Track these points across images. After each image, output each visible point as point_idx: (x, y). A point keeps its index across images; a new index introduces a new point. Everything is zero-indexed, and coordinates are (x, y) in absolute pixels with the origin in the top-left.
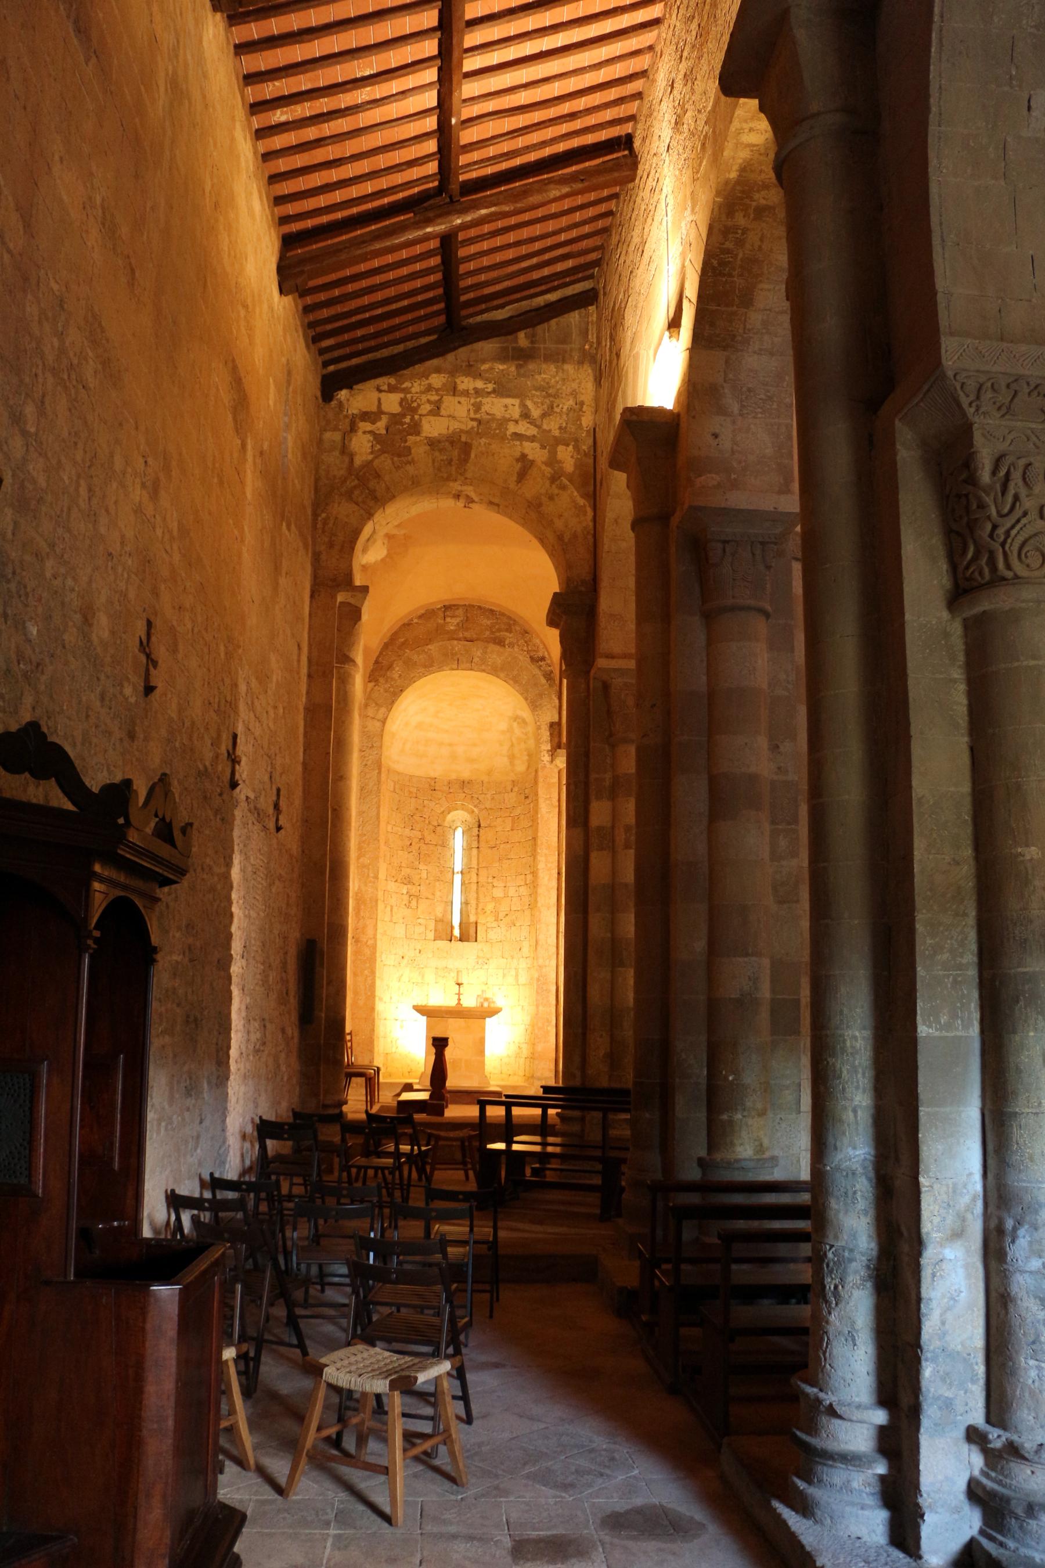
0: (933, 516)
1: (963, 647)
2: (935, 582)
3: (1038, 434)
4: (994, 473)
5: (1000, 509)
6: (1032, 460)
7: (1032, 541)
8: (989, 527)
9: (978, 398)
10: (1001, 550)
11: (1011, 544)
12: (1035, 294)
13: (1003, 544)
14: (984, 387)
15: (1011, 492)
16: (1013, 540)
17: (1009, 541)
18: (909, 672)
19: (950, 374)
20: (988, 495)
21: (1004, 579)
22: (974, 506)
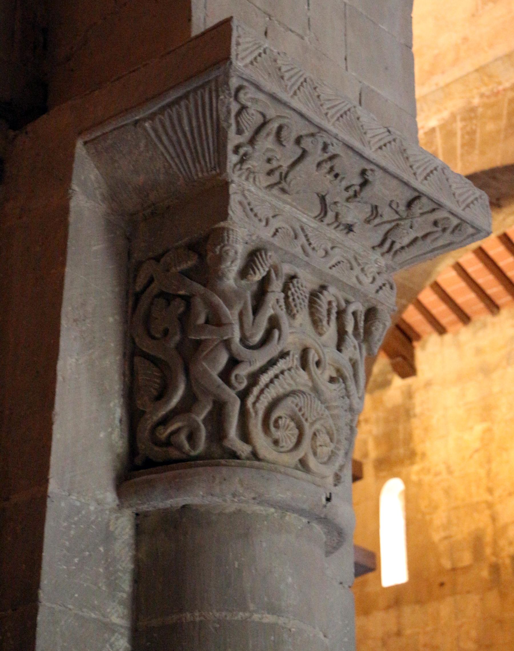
1: (131, 566)
2: (102, 435)
3: (310, 235)
4: (243, 273)
5: (248, 334)
8: (223, 359)
9: (252, 141)
10: (238, 403)
11: (258, 398)
12: (308, 32)
13: (244, 395)
15: (268, 311)
16: (262, 391)
17: (256, 391)
18: (42, 595)
19: (234, 82)
20: (230, 306)
21: (234, 455)
22: (201, 320)
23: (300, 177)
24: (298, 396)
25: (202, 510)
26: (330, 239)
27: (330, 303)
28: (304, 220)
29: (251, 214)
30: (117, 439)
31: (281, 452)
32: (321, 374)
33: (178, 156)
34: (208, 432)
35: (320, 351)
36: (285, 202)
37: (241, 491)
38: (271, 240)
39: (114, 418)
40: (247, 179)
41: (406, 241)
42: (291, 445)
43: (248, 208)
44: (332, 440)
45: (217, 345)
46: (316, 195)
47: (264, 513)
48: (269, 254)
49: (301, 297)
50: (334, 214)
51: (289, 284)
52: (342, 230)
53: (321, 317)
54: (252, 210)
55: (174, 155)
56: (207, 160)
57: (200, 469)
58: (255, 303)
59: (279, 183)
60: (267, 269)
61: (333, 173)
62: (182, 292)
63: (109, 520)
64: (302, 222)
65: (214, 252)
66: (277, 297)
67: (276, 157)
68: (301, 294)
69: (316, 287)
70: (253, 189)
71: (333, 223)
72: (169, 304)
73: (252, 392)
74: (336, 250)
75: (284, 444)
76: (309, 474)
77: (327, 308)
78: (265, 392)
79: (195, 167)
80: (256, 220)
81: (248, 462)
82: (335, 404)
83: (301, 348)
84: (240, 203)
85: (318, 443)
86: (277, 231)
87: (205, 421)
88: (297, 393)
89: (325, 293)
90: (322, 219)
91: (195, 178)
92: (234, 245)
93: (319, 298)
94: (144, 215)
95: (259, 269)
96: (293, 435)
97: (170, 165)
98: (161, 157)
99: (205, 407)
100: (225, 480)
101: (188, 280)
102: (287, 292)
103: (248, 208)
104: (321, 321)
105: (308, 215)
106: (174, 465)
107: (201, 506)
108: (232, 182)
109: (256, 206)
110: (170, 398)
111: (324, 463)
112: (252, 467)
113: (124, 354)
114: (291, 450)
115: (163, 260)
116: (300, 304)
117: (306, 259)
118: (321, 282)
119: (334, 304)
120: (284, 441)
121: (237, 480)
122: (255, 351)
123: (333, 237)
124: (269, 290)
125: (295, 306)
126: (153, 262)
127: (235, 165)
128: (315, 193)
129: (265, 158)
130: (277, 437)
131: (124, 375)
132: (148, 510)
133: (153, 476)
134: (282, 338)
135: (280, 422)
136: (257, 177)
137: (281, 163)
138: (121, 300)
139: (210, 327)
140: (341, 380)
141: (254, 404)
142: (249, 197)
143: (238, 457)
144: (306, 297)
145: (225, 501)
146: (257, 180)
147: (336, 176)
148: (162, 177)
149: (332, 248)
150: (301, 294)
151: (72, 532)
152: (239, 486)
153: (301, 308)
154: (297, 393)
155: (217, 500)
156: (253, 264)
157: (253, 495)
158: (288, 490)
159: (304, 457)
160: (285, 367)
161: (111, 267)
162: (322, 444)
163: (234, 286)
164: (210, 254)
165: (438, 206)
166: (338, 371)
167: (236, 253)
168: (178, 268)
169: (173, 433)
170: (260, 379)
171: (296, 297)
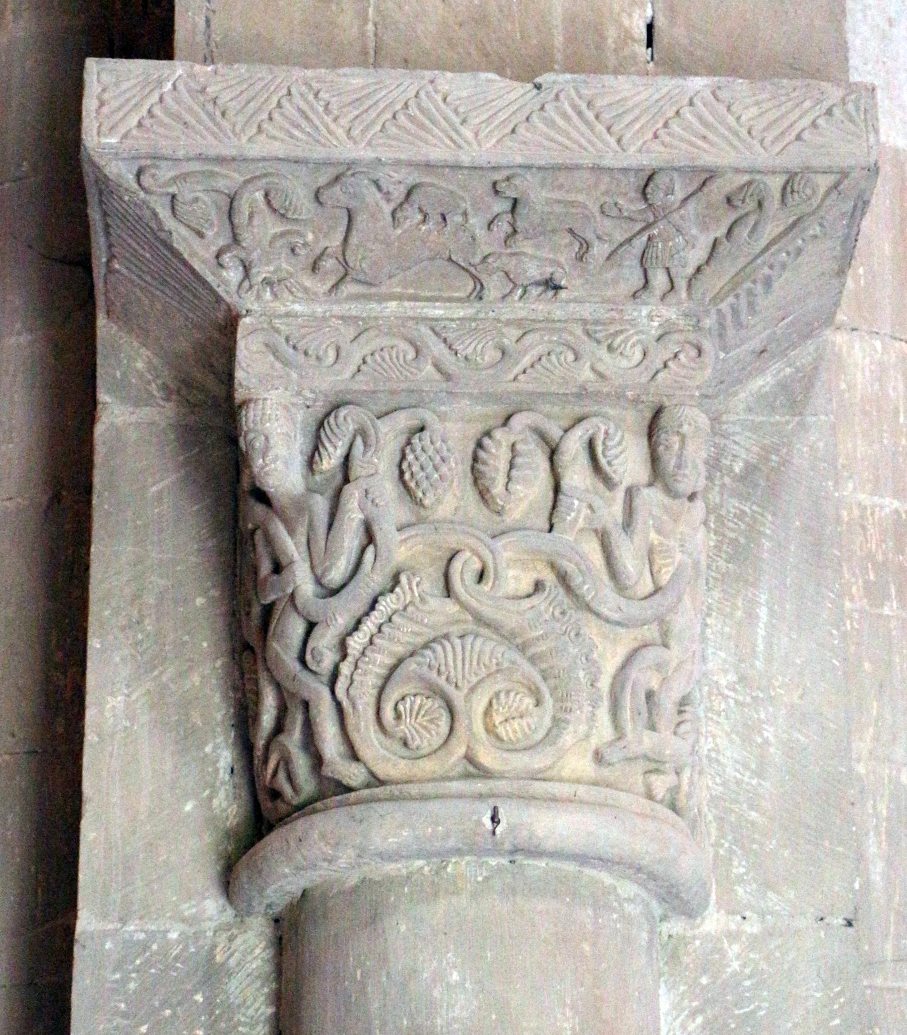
3: (451, 336)
6: (428, 416)
7: (411, 666)
14: (243, 208)
40: (275, 295)
41: (696, 256)
63: (214, 946)
75: (418, 742)
81: (365, 792)
92: (259, 427)
151: (132, 986)
161: (195, 508)
165: (709, 176)
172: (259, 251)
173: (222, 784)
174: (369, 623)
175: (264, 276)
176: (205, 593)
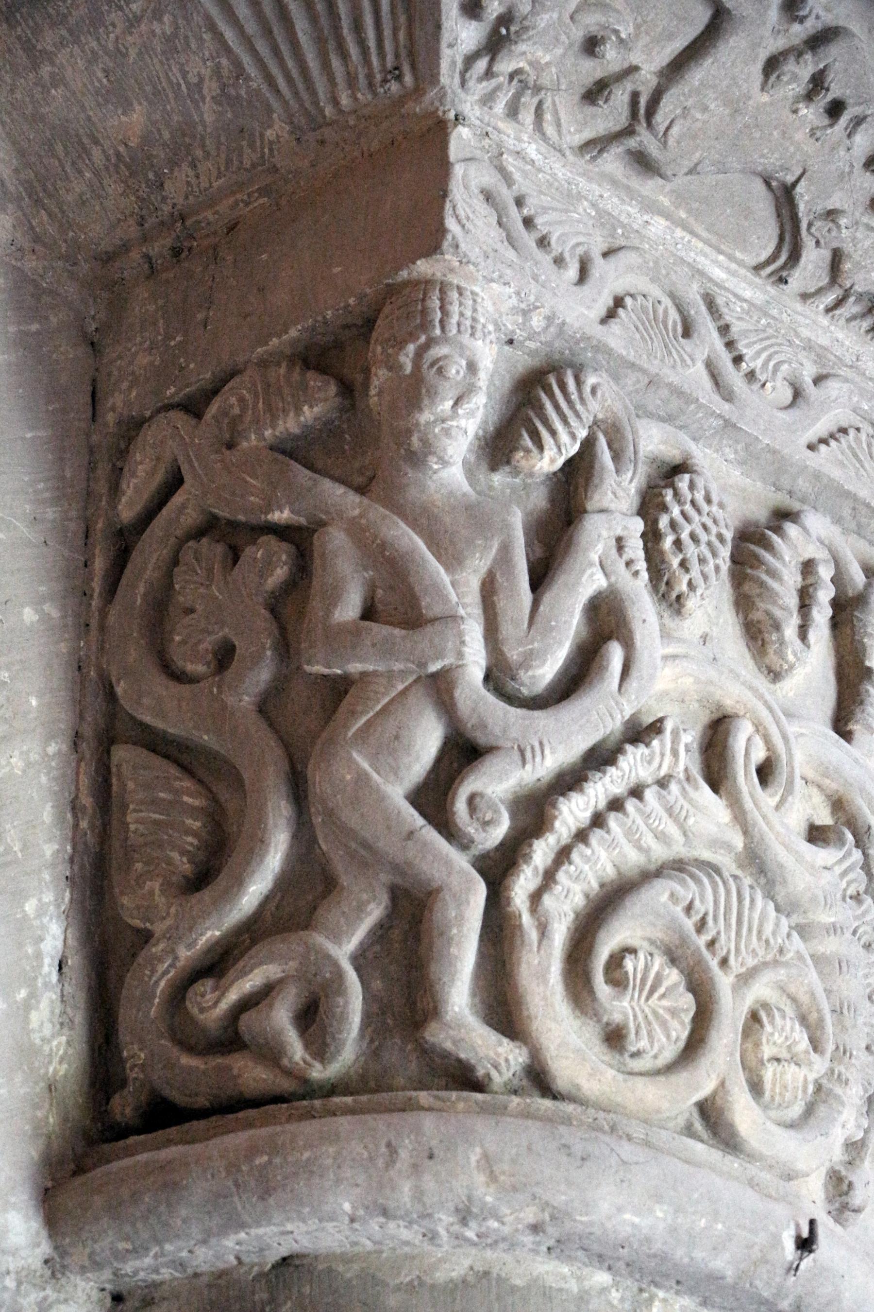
0: (29, 615)
3: (737, 328)
5: (513, 654)
10: (480, 892)
11: (549, 877)
16: (563, 855)
23: (705, 109)
24: (692, 876)
25: (350, 1272)
26: (809, 346)
27: (808, 567)
28: (718, 274)
29: (529, 240)
30: (47, 1030)
31: (631, 1073)
32: (777, 808)
33: (268, 32)
34: (369, 996)
35: (774, 731)
36: (650, 207)
37: (489, 1199)
38: (598, 331)
39: (39, 955)
40: (513, 111)
42: (669, 1053)
43: (515, 216)
44: (816, 1045)
45: (404, 693)
46: (759, 186)
47: (573, 1286)
48: (591, 380)
49: (703, 537)
50: (826, 254)
51: (664, 492)
52: (853, 318)
53: (778, 613)
54: (528, 222)
55: (251, 27)
56: (372, 43)
57: (344, 1122)
58: (539, 552)
59: (629, 131)
60: (583, 434)
61: (824, 100)
62: (281, 516)
64: (710, 280)
65: (394, 367)
66: (619, 532)
67: (616, 32)
68: (705, 527)
69: (760, 514)
70: (532, 150)
71: (819, 291)
72: (236, 560)
73: (527, 858)
74: (833, 387)
75: (643, 1044)
76: (737, 1157)
77: (799, 587)
78: (575, 856)
79: (326, 65)
80: (546, 259)
82: (826, 918)
83: (705, 718)
84: (488, 196)
85: (767, 1051)
86: (619, 302)
87: (359, 960)
88: (690, 868)
89: (791, 529)
90: (784, 274)
91: (329, 111)
92: (465, 339)
93: (768, 546)
94: (148, 258)
95: (553, 433)
96: (674, 1012)
97: (237, 64)
98: (207, 36)
99: (361, 909)
100: (431, 1157)
101: (302, 475)
102: (656, 522)
103: (515, 216)
104: (777, 626)
105: (731, 258)
106: (252, 1113)
107: (346, 1259)
108: (459, 119)
109: (545, 210)
110: (239, 883)
111: (792, 1126)
112: (527, 1114)
113: (76, 740)
114: (670, 1068)
115: (213, 409)
116: (702, 561)
117: (725, 408)
118: (782, 500)
119: (825, 572)
120: (644, 1032)
121: (473, 1159)
122: (537, 713)
123: (823, 340)
124: (589, 506)
125: (683, 564)
126: (178, 418)
127: (470, 60)
128: (760, 175)
129: (578, 34)
130: (617, 1018)
131: (75, 806)
132: (155, 1277)
133: (173, 1152)
134: (634, 673)
135: (629, 963)
136: (548, 104)
137: (635, 58)
138: (66, 553)
139: (379, 630)
140: (849, 837)
141: (536, 898)
142: (517, 176)
143: (478, 1086)
144: (721, 538)
145: (432, 1237)
146: (548, 117)
147: (835, 109)
148: (208, 113)
149: (818, 380)
150: (705, 527)
152: (480, 1179)
153: (705, 577)
154: (690, 868)
155: (405, 1234)
156: (531, 414)
157: (530, 1215)
158: (658, 1198)
159: (714, 1094)
160: (645, 774)
162: (784, 1054)
163: (466, 487)
164: (380, 376)
166: (838, 805)
167: (472, 367)
168: (268, 433)
169: (247, 1004)
170: (558, 809)
171: (685, 536)
172: (555, 15)
173: (46, 985)
174: (599, 785)
175: (521, 65)
176: (37, 603)
